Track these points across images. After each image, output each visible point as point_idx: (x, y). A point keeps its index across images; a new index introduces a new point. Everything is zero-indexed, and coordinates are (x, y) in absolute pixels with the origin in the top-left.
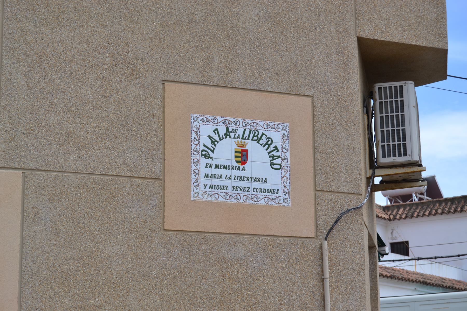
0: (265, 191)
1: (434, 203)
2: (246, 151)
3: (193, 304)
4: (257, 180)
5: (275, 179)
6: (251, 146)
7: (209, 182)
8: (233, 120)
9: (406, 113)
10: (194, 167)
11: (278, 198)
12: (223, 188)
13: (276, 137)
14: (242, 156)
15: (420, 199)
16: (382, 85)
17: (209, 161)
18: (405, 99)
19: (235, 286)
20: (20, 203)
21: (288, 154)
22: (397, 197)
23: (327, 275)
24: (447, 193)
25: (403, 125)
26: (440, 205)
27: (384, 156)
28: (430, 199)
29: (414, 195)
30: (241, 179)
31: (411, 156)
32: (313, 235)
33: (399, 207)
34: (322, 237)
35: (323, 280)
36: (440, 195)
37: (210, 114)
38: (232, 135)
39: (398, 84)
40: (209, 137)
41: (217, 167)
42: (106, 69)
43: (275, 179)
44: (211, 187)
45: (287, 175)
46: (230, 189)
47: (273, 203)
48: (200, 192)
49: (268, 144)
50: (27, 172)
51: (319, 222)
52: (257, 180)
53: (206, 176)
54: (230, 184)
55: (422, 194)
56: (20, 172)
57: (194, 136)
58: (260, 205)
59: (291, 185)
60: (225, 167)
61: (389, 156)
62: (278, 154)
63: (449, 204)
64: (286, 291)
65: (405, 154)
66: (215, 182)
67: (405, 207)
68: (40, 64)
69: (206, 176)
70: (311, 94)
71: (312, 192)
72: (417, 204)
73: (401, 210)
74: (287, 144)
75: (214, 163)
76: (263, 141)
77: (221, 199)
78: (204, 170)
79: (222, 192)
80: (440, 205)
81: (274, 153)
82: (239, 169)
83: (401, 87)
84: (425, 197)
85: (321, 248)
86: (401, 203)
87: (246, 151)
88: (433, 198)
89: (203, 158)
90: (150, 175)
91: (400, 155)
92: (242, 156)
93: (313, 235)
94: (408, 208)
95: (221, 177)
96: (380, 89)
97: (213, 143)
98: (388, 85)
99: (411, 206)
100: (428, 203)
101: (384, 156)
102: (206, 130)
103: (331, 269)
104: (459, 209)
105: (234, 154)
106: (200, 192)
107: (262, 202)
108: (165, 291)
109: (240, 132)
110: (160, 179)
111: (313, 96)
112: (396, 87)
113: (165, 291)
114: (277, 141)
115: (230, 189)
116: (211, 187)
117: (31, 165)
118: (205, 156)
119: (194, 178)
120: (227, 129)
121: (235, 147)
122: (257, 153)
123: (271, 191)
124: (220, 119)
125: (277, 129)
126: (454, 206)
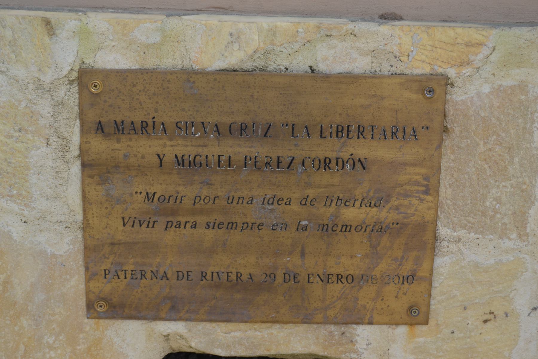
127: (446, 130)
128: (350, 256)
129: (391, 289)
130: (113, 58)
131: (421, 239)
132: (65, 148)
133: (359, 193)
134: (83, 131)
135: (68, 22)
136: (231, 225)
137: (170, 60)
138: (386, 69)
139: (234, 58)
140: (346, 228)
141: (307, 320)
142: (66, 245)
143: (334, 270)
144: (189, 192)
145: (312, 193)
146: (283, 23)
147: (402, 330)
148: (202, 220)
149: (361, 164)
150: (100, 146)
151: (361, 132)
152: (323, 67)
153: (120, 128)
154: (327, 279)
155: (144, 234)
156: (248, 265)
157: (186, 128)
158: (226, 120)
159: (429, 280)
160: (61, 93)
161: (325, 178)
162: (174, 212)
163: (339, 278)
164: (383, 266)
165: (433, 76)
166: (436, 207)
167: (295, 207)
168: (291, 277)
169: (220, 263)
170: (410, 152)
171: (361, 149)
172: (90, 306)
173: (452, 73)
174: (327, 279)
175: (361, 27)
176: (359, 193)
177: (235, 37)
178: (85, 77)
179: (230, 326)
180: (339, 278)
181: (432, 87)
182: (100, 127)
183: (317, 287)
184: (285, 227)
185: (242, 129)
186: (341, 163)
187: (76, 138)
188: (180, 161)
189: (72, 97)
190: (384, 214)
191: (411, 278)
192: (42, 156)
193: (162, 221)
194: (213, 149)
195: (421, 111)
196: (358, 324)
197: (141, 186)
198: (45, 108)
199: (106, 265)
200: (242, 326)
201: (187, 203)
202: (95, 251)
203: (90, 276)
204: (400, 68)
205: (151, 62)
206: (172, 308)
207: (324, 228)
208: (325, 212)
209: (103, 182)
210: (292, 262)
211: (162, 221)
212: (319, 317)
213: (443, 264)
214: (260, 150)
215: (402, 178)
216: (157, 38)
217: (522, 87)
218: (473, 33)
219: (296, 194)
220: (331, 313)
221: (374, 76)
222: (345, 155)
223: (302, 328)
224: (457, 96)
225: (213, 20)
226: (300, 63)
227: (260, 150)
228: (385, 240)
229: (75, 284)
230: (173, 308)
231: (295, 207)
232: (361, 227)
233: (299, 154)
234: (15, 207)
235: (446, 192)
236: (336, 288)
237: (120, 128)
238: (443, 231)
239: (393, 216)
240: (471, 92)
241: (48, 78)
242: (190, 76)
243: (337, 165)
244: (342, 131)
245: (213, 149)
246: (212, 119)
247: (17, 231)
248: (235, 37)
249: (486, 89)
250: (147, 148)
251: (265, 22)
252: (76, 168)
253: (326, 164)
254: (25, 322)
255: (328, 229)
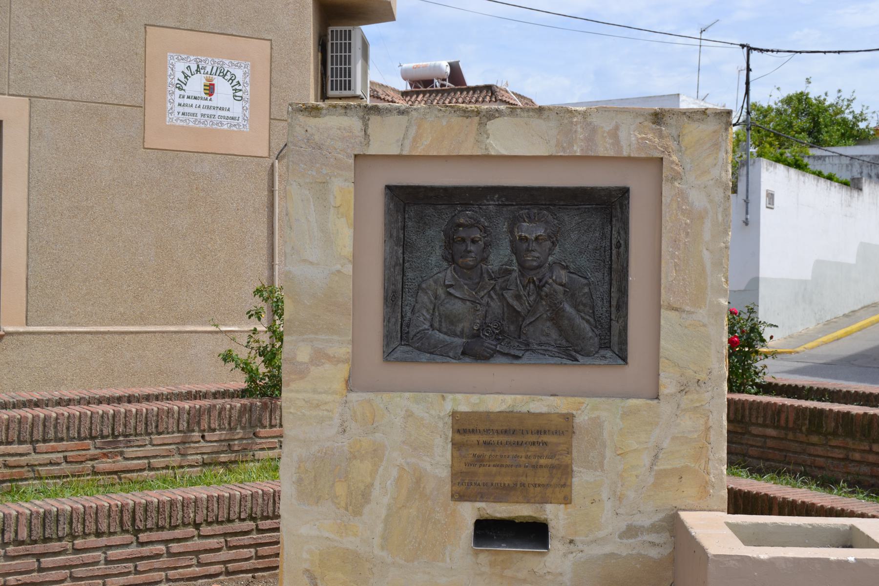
0: (228, 118)
1: (455, 91)
2: (213, 85)
3: (167, 208)
4: (221, 109)
5: (237, 109)
6: (218, 82)
7: (182, 109)
8: (203, 58)
9: (352, 54)
10: (169, 98)
11: (238, 124)
12: (193, 115)
13: (239, 74)
14: (210, 89)
15: (442, 85)
16: (335, 28)
17: (182, 92)
18: (352, 42)
19: (201, 194)
20: (28, 125)
21: (248, 88)
22: (419, 82)
23: (277, 188)
24: (471, 80)
25: (350, 64)
26: (461, 93)
27: (332, 89)
28: (452, 86)
29: (436, 81)
30: (209, 108)
31: (355, 90)
32: (266, 155)
33: (418, 93)
34: (273, 157)
35: (273, 191)
36: (465, 84)
37: (184, 53)
38: (202, 71)
39: (347, 28)
40: (183, 72)
41: (188, 97)
42: (97, 14)
43: (237, 109)
44: (183, 114)
45: (247, 106)
46: (199, 116)
47: (234, 128)
48: (174, 118)
49: (232, 80)
50: (33, 99)
51: (272, 144)
52: (221, 109)
53: (180, 105)
54: (199, 111)
55: (444, 80)
56: (27, 99)
57: (170, 71)
58: (223, 130)
59: (250, 113)
60: (195, 98)
61: (337, 89)
62: (240, 88)
63: (471, 92)
64: (242, 199)
65: (350, 89)
66: (187, 110)
67: (424, 93)
68: (43, 9)
69: (180, 105)
70: (270, 38)
71: (268, 120)
72: (437, 92)
73: (421, 96)
74: (248, 79)
75: (186, 95)
76: (228, 77)
77: (191, 124)
78: (178, 100)
79: (192, 119)
80: (461, 93)
81: (237, 87)
82: (206, 99)
83: (350, 31)
84: (447, 83)
85: (273, 165)
86: (422, 89)
87: (213, 85)
88: (456, 85)
89: (177, 90)
90: (133, 103)
91: (345, 89)
92: (210, 89)
93: (266, 155)
94: (428, 95)
95: (192, 106)
96: (332, 31)
97: (186, 77)
98: (339, 28)
99: (431, 92)
100: (449, 91)
101: (332, 89)
102: (180, 67)
103: (280, 182)
104: (480, 99)
105: (203, 87)
106: (174, 118)
107: (225, 127)
108: (144, 196)
109: (209, 69)
110: (142, 107)
111: (271, 40)
112: (345, 31)
113: (144, 196)
114: (240, 77)
115: (199, 116)
116: (183, 114)
117: (36, 93)
118: (179, 88)
119: (169, 106)
120: (198, 66)
121: (204, 81)
122: (223, 87)
123: (233, 118)
124: (192, 58)
125: (240, 67)
126: (476, 96)
127: (574, 432)
128: (542, 477)
129: (557, 489)
130: (464, 408)
131: (566, 471)
132: (446, 439)
133: (545, 453)
134: (453, 433)
135: (450, 397)
136: (502, 466)
137: (482, 409)
138: (553, 411)
139: (503, 408)
140: (541, 466)
141: (528, 502)
142: (445, 473)
143: (537, 482)
144: (488, 454)
145: (529, 454)
146: (518, 396)
147: (562, 506)
148: (492, 464)
149: (545, 443)
150: (458, 437)
151: (545, 432)
152: (532, 411)
153: (465, 431)
154: (535, 485)
155: (472, 469)
156: (507, 480)
157: (487, 431)
158: (500, 428)
159: (571, 486)
160: (446, 420)
161: (533, 449)
162: (482, 461)
163: (539, 485)
164: (555, 481)
165: (567, 414)
166: (572, 459)
167: (523, 459)
168: (523, 485)
169: (498, 480)
170: (562, 439)
171: (545, 438)
172: (452, 496)
173: (574, 412)
174: (535, 485)
175: (543, 398)
176: (545, 453)
177: (503, 401)
178: (454, 414)
179: (502, 504)
180: (539, 485)
181: (568, 418)
182: (458, 431)
183: (532, 488)
184: (520, 466)
185: (506, 431)
186: (539, 443)
187: (450, 435)
188: (485, 443)
189: (449, 421)
190: (554, 461)
191: (564, 485)
192: (439, 441)
193: (478, 464)
194: (496, 438)
195: (565, 426)
196: (546, 503)
197: (471, 452)
198: (441, 424)
199: (459, 480)
200: (506, 504)
201: (487, 457)
202: (456, 475)
203: (453, 484)
204: (557, 411)
205: (476, 409)
206: (481, 496)
207: (533, 467)
208: (534, 461)
209: (459, 450)
210: (523, 479)
211: (478, 464)
212: (533, 500)
213: (576, 481)
214: (512, 439)
215: (560, 449)
216: (478, 401)
217: (598, 417)
218: (581, 399)
219: (524, 454)
220: (537, 499)
221: (549, 413)
222: (540, 440)
223: (526, 505)
224: (577, 420)
225: (496, 396)
226: (524, 409)
227: (512, 439)
228: (554, 471)
229: (447, 488)
230: (482, 497)
231: (523, 459)
232: (546, 466)
233: (525, 440)
234: (428, 459)
235: (575, 454)
236: (538, 489)
237: (465, 431)
238: (575, 468)
239: (557, 462)
240: (582, 419)
241: (442, 414)
242: (488, 414)
243: (787, 418)
244: (539, 432)
245: (496, 438)
246: (495, 428)
247: (429, 468)
248: (503, 401)
249: (586, 418)
250: (474, 438)
251: (513, 396)
252: (450, 445)
253: (534, 443)
254: (429, 502)
255: (535, 467)
